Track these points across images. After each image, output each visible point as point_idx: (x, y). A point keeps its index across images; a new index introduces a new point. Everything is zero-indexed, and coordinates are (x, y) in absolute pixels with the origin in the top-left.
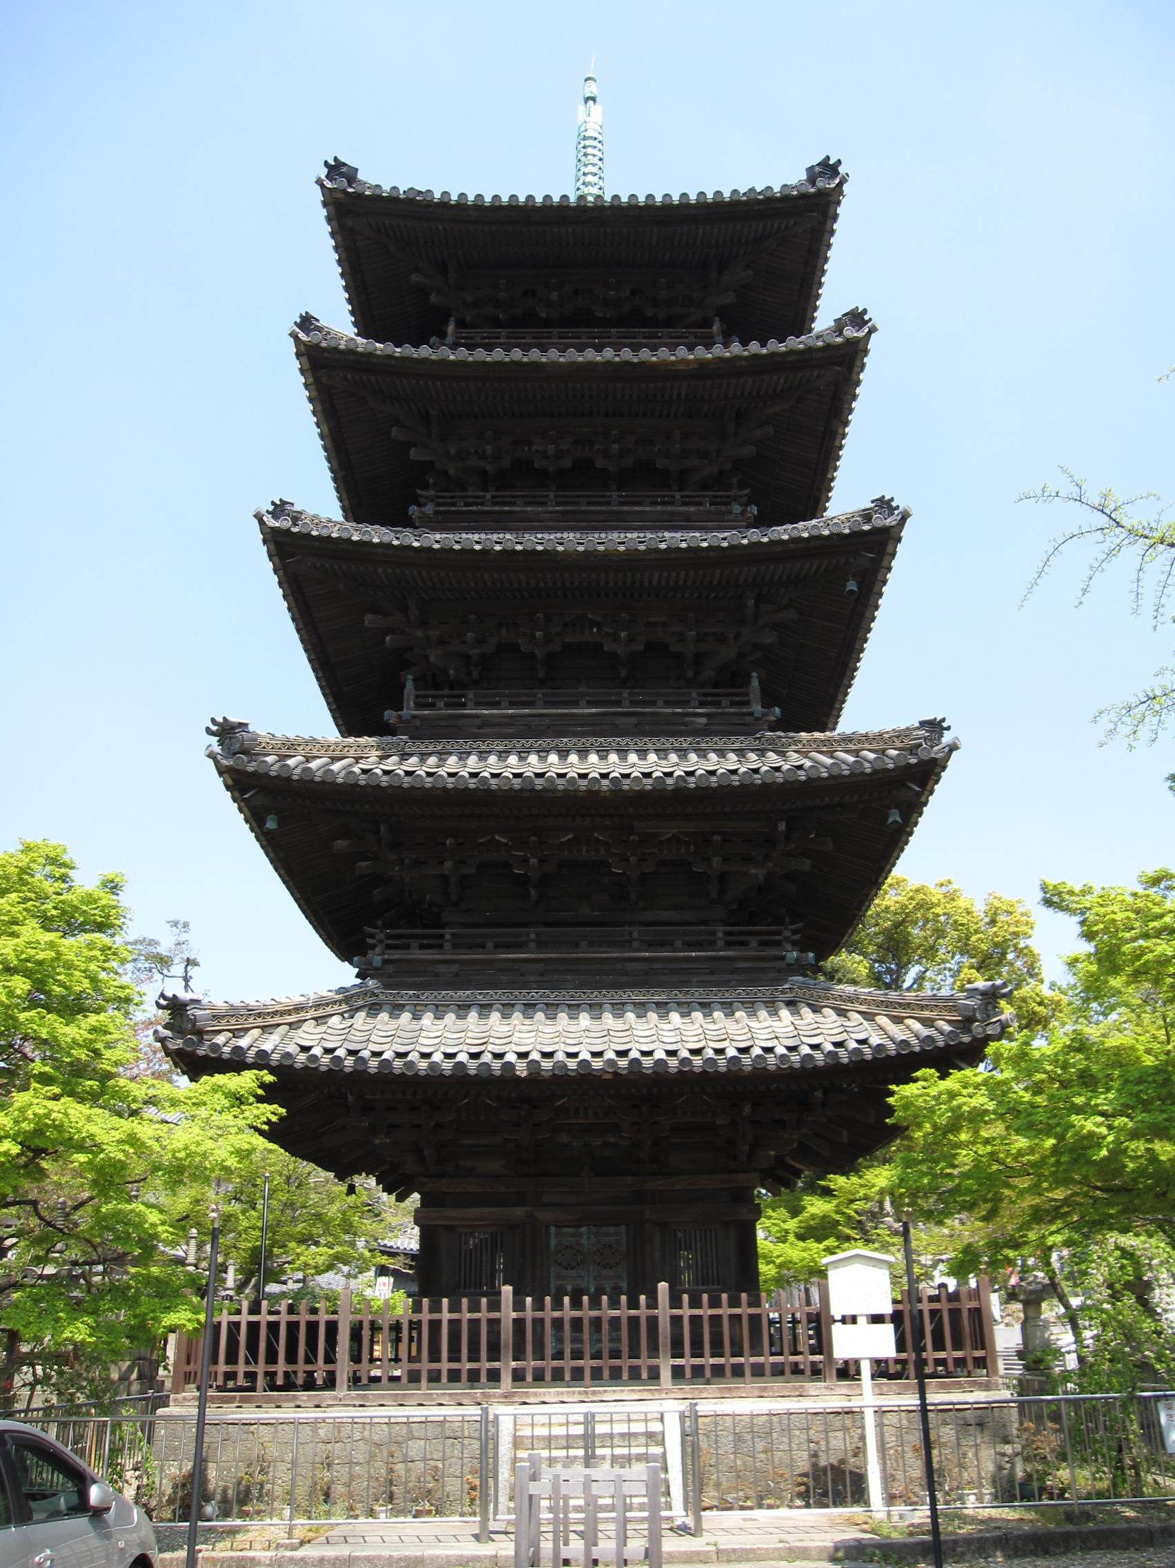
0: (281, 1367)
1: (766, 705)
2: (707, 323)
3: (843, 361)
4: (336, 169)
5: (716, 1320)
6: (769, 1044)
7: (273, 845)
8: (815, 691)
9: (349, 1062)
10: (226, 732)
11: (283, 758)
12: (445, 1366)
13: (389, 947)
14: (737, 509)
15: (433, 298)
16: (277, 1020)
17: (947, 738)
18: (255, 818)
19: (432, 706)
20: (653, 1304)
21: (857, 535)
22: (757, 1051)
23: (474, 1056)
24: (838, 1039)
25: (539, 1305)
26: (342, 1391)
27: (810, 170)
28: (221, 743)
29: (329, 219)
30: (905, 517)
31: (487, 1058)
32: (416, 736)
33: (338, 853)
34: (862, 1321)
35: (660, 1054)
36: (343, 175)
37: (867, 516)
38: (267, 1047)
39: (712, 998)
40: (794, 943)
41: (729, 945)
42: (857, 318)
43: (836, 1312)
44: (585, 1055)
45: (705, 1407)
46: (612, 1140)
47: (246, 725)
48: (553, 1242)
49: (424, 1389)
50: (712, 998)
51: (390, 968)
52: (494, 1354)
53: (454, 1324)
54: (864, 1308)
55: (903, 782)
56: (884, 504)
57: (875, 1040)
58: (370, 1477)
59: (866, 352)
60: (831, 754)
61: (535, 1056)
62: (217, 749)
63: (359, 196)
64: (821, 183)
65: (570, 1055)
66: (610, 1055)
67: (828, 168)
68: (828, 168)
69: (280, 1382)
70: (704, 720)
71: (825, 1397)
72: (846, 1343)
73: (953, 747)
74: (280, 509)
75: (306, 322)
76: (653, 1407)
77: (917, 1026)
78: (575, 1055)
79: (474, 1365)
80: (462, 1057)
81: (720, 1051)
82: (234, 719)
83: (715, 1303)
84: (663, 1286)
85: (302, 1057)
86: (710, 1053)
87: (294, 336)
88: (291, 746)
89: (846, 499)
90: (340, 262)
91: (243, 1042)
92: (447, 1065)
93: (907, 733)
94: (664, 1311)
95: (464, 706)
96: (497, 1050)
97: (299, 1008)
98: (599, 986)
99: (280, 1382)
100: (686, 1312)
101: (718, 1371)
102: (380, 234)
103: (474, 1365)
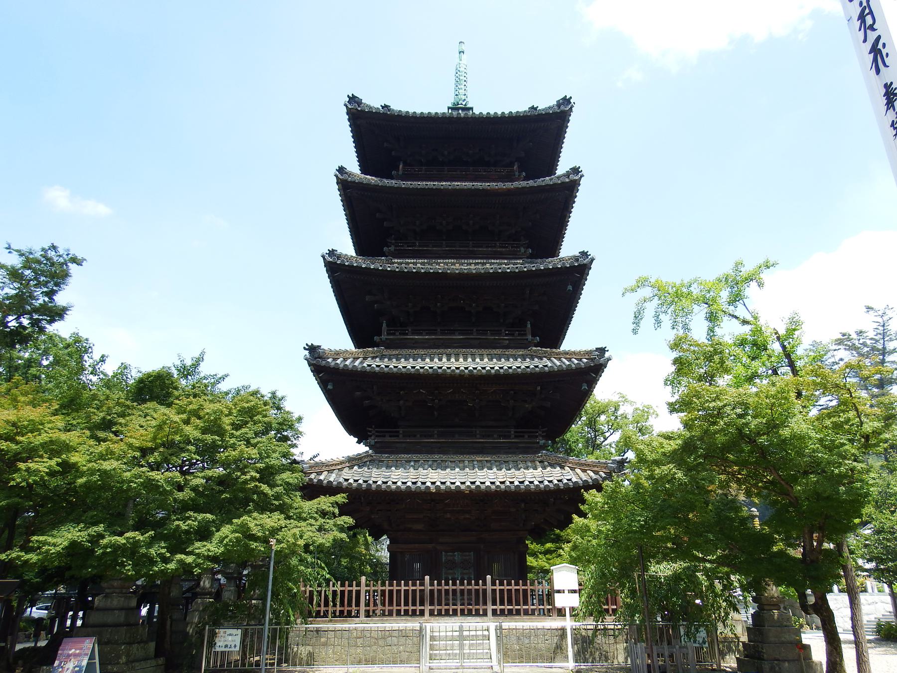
0: (338, 608)
1: (534, 335)
2: (511, 164)
3: (569, 189)
4: (353, 99)
5: (509, 591)
6: (531, 480)
9: (364, 485)
10: (313, 349)
11: (335, 359)
12: (403, 608)
13: (377, 436)
14: (523, 250)
15: (393, 153)
16: (334, 468)
17: (607, 355)
18: (323, 384)
19: (394, 334)
20: (485, 583)
21: (572, 267)
22: (527, 483)
23: (414, 483)
24: (559, 478)
25: (439, 584)
26: (362, 617)
27: (558, 101)
28: (310, 353)
29: (349, 120)
30: (592, 260)
31: (419, 484)
32: (388, 347)
34: (566, 592)
35: (488, 484)
36: (355, 102)
37: (576, 259)
38: (332, 479)
39: (509, 459)
40: (543, 436)
41: (516, 437)
42: (576, 170)
43: (556, 588)
44: (458, 484)
45: (505, 625)
46: (467, 516)
48: (444, 559)
49: (395, 617)
50: (509, 459)
51: (378, 445)
52: (422, 604)
53: (406, 591)
54: (566, 587)
55: (593, 367)
56: (584, 254)
57: (574, 480)
60: (559, 359)
61: (438, 483)
62: (308, 356)
63: (363, 111)
64: (562, 108)
65: (452, 483)
66: (468, 483)
67: (566, 101)
68: (566, 101)
69: (338, 614)
71: (554, 623)
72: (560, 601)
73: (609, 359)
74: (332, 253)
75: (341, 170)
76: (485, 625)
77: (592, 474)
78: (454, 483)
79: (414, 608)
80: (409, 484)
81: (512, 483)
82: (316, 344)
83: (509, 584)
84: (489, 577)
85: (345, 483)
86: (508, 483)
87: (336, 176)
88: (338, 353)
89: (569, 249)
90: (352, 131)
91: (322, 477)
92: (403, 487)
93: (591, 352)
94: (489, 587)
95: (407, 334)
96: (423, 481)
97: (342, 463)
98: (462, 453)
99: (338, 614)
100: (498, 587)
101: (510, 612)
102: (375, 131)
103: (414, 608)
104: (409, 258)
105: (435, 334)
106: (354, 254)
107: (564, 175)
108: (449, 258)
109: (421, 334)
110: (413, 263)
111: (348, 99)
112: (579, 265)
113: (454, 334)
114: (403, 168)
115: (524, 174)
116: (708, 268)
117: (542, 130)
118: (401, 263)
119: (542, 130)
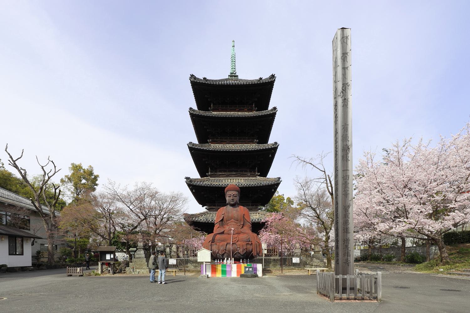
7: (194, 194)
8: (264, 172)
10: (187, 178)
13: (209, 206)
15: (209, 100)
17: (281, 180)
19: (213, 172)
33: (201, 193)
41: (252, 206)
42: (275, 108)
47: (190, 178)
55: (275, 185)
58: (442, 192)
59: (276, 114)
67: (273, 76)
70: (249, 175)
75: (191, 109)
88: (195, 179)
89: (271, 141)
102: (204, 91)
104: (216, 144)
105: (226, 172)
106: (198, 143)
107: (270, 110)
108: (230, 144)
109: (221, 172)
110: (218, 146)
111: (190, 76)
112: (273, 113)
113: (232, 172)
114: (213, 106)
115: (257, 108)
116: (272, 74)
117: (261, 91)
118: (214, 146)
119: (261, 91)
